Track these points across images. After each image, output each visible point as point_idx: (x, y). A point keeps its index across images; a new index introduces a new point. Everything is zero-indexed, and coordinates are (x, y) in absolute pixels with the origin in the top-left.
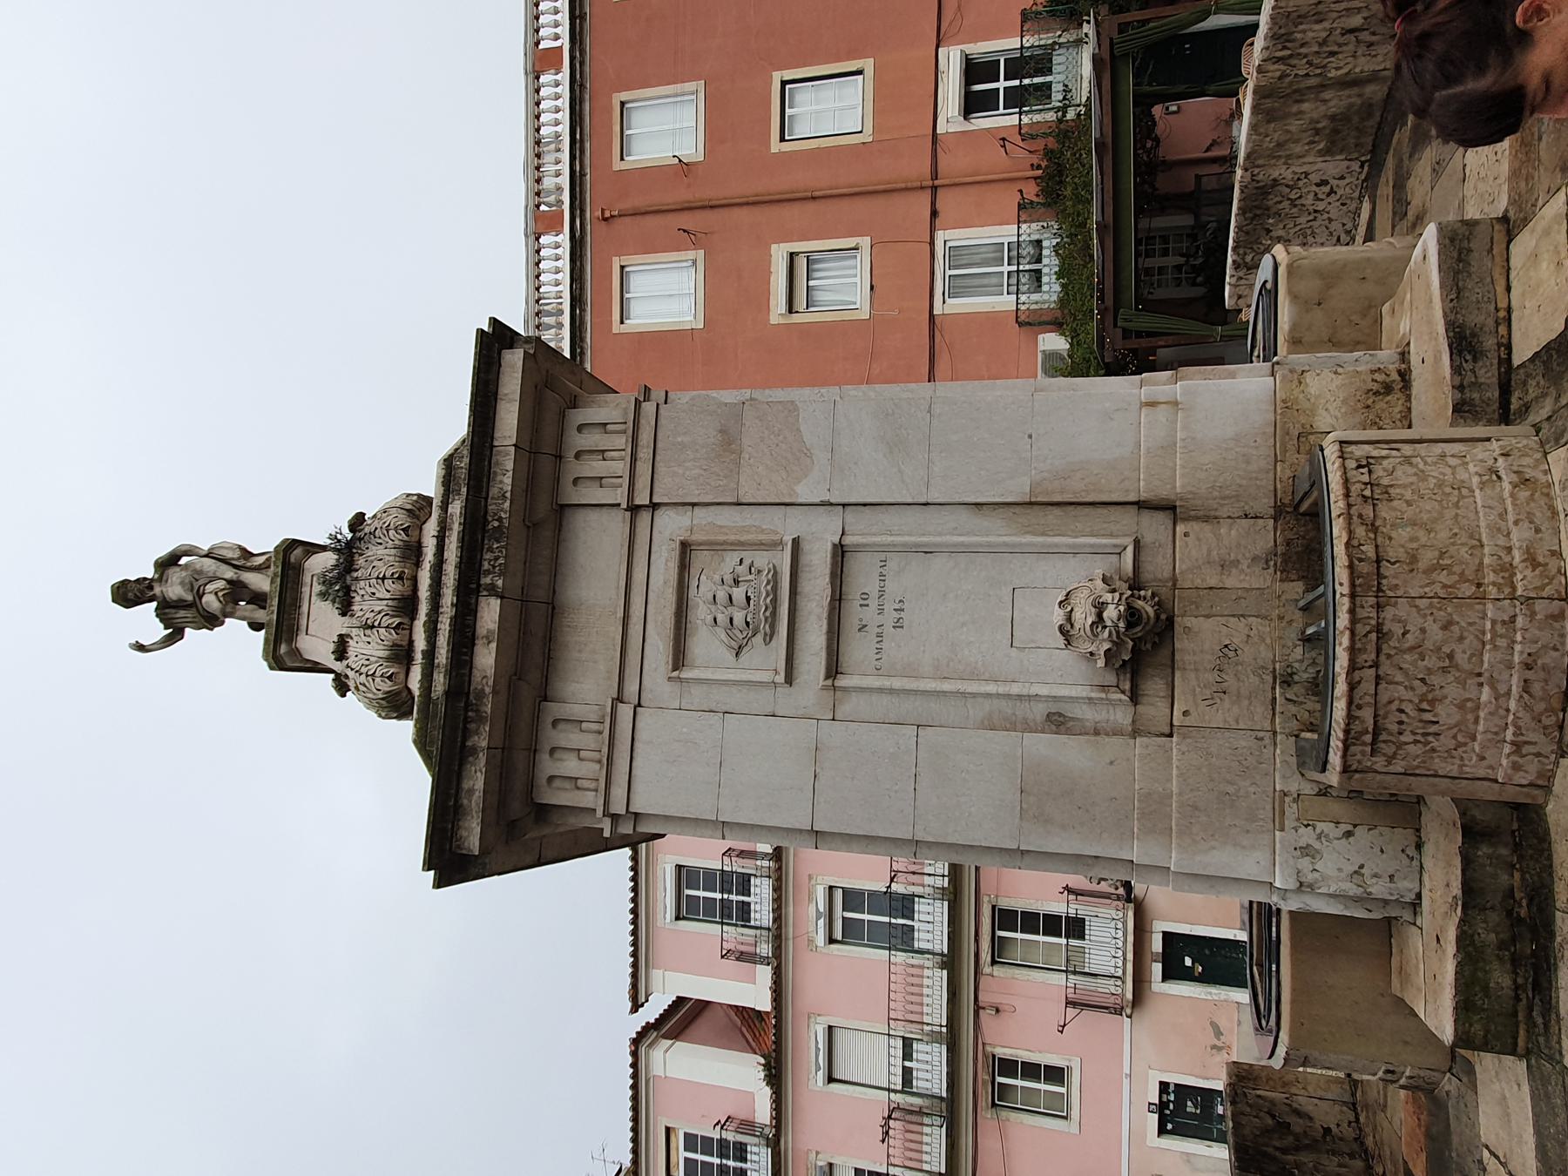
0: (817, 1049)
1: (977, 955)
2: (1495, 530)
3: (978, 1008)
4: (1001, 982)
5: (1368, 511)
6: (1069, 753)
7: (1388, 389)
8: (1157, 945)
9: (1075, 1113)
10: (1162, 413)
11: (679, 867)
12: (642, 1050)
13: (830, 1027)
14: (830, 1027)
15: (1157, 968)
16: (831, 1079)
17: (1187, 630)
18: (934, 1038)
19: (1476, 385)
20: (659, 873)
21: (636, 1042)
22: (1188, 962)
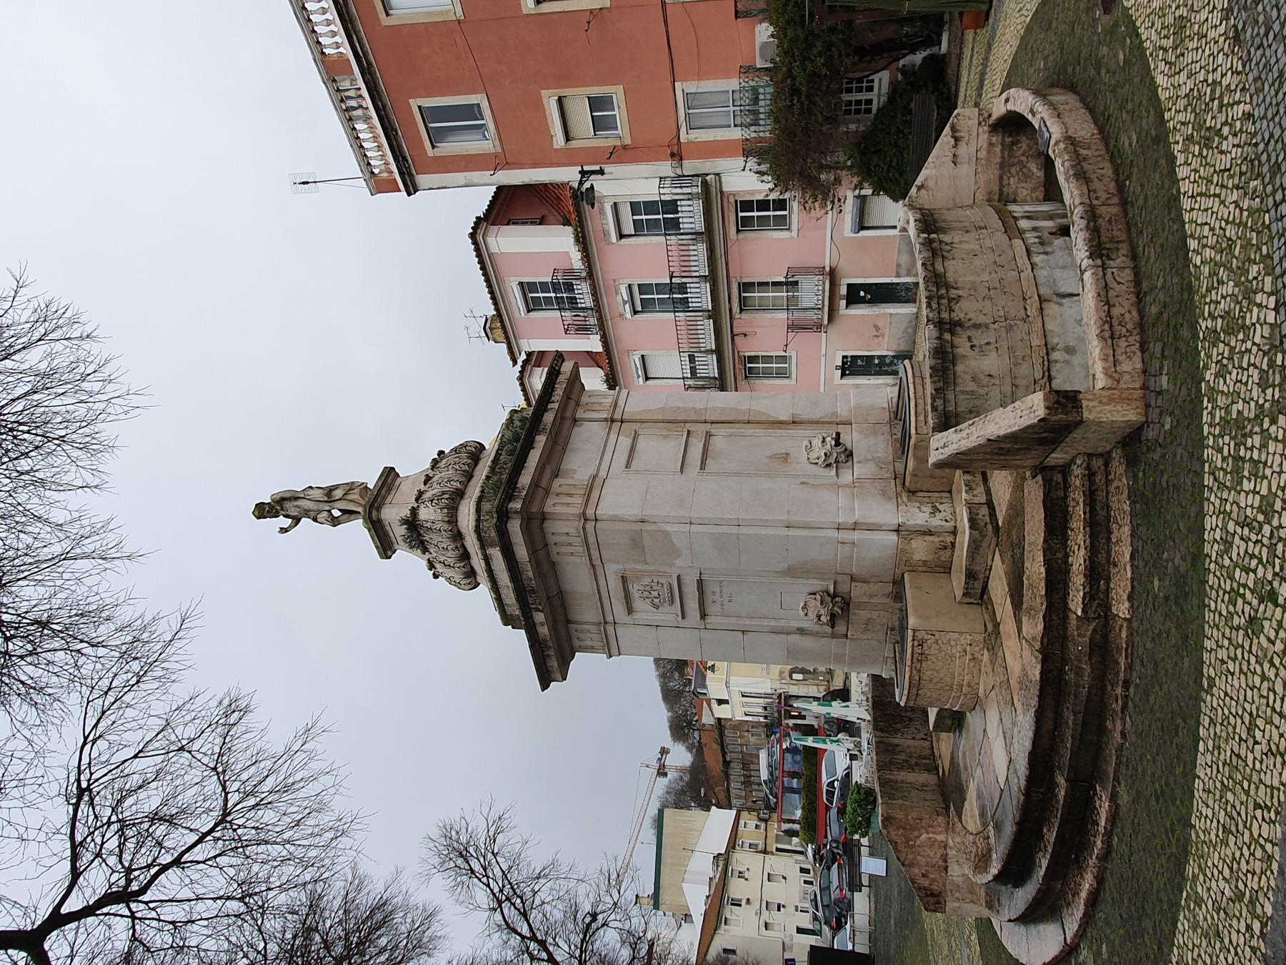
0: (637, 368)
1: (731, 310)
2: (960, 674)
4: (744, 321)
5: (919, 666)
6: (807, 642)
7: (945, 548)
8: (844, 291)
9: (794, 376)
10: (847, 547)
11: (521, 284)
12: (526, 380)
13: (643, 356)
14: (643, 356)
15: (843, 303)
16: (647, 378)
17: (855, 614)
19: (973, 588)
20: (509, 291)
21: (473, 236)
22: (862, 294)
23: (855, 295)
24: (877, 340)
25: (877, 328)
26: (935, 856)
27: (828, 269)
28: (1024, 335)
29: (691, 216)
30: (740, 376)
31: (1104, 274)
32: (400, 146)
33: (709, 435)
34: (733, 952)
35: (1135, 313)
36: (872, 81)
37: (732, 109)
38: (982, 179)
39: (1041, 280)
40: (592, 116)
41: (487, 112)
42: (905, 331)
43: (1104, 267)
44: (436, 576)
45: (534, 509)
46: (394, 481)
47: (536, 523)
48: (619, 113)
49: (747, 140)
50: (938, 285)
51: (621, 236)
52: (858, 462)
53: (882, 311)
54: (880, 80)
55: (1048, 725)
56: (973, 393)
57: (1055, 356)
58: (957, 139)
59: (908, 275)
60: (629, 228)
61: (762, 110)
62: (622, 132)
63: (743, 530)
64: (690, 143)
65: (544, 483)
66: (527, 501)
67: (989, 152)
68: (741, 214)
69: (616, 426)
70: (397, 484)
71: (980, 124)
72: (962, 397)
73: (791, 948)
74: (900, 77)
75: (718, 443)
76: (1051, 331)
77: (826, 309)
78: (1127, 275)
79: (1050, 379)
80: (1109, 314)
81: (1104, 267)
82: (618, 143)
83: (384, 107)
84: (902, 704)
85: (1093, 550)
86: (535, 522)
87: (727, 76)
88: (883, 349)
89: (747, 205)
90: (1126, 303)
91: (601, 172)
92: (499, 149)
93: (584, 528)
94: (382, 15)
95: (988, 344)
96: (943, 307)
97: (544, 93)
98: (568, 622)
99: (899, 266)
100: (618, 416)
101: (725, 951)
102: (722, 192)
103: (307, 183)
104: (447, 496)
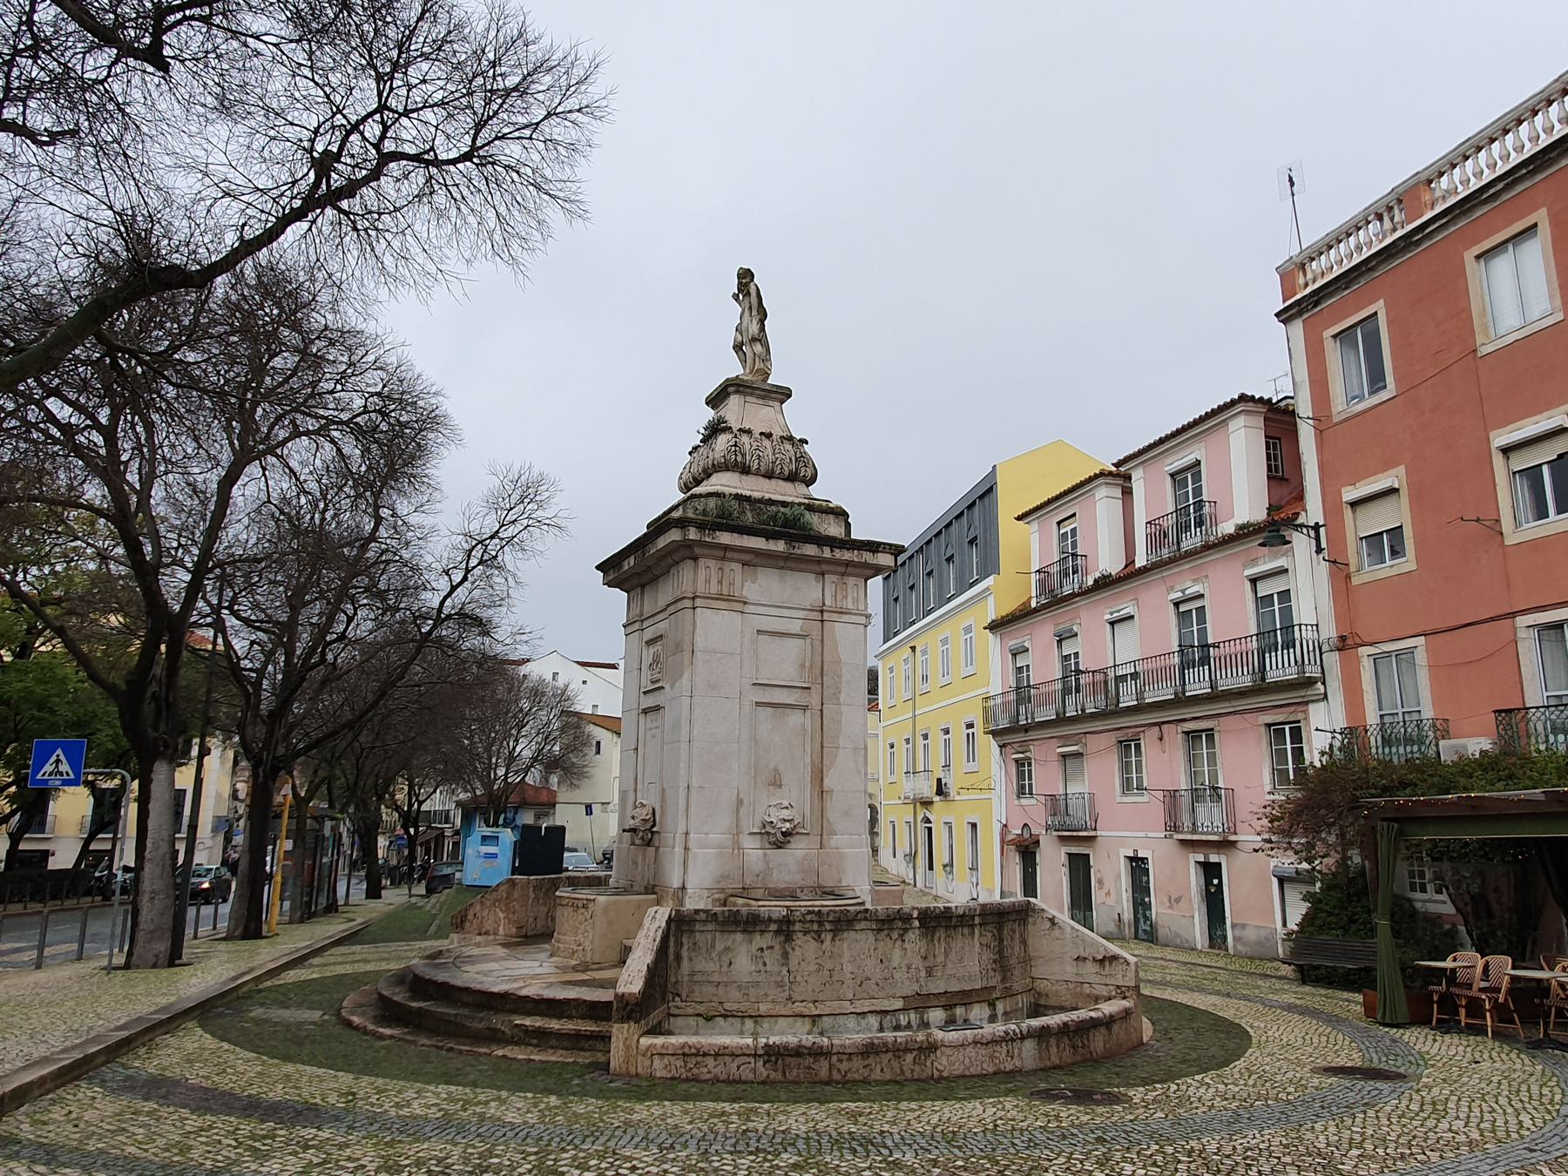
1: (1184, 720)
3: (1159, 724)
4: (1175, 735)
8: (1213, 858)
9: (1125, 799)
11: (1198, 463)
12: (1101, 480)
13: (1287, 570)
14: (1132, 617)
16: (1112, 624)
18: (1140, 695)
20: (1188, 451)
21: (1243, 398)
23: (1211, 871)
24: (1166, 900)
25: (1178, 900)
26: (488, 925)
27: (1233, 838)
28: (772, 997)
29: (1280, 669)
30: (1121, 735)
31: (749, 1055)
32: (1331, 295)
33: (805, 708)
34: (598, 752)
35: (708, 1076)
36: (1439, 892)
37: (1400, 711)
38: (1061, 988)
39: (841, 1020)
40: (1381, 533)
41: (1376, 399)
42: (1178, 935)
43: (755, 1055)
44: (690, 453)
45: (697, 550)
46: (774, 399)
47: (688, 553)
48: (1390, 567)
49: (1366, 731)
50: (836, 922)
51: (1254, 581)
52: (765, 854)
53: (1196, 906)
54: (1445, 903)
55: (467, 999)
56: (713, 947)
57: (749, 1024)
58: (1102, 962)
59: (1234, 938)
60: (1264, 589)
61: (1394, 750)
62: (1367, 572)
63: (684, 746)
64: (1358, 659)
65: (729, 555)
66: (700, 543)
67: (1089, 996)
68: (1287, 728)
69: (817, 616)
70: (771, 403)
71: (1118, 987)
72: (709, 936)
73: (605, 811)
74: (1447, 927)
75: (795, 718)
76: (776, 1022)
77: (1195, 837)
78: (747, 1074)
79: (725, 1016)
80: (705, 1055)
81: (755, 1055)
82: (1352, 568)
83: (1371, 269)
84: (557, 893)
85: (559, 1035)
86: (687, 552)
87: (1436, 704)
88: (1158, 909)
89: (1297, 735)
90: (717, 1070)
91: (1319, 550)
92: (1336, 419)
93: (683, 598)
94: (1477, 250)
95: (765, 964)
96: (807, 925)
97: (1401, 470)
98: (643, 587)
99: (1244, 926)
100: (826, 616)
101: (598, 743)
102: (1307, 703)
103: (1292, 184)
104: (739, 459)
